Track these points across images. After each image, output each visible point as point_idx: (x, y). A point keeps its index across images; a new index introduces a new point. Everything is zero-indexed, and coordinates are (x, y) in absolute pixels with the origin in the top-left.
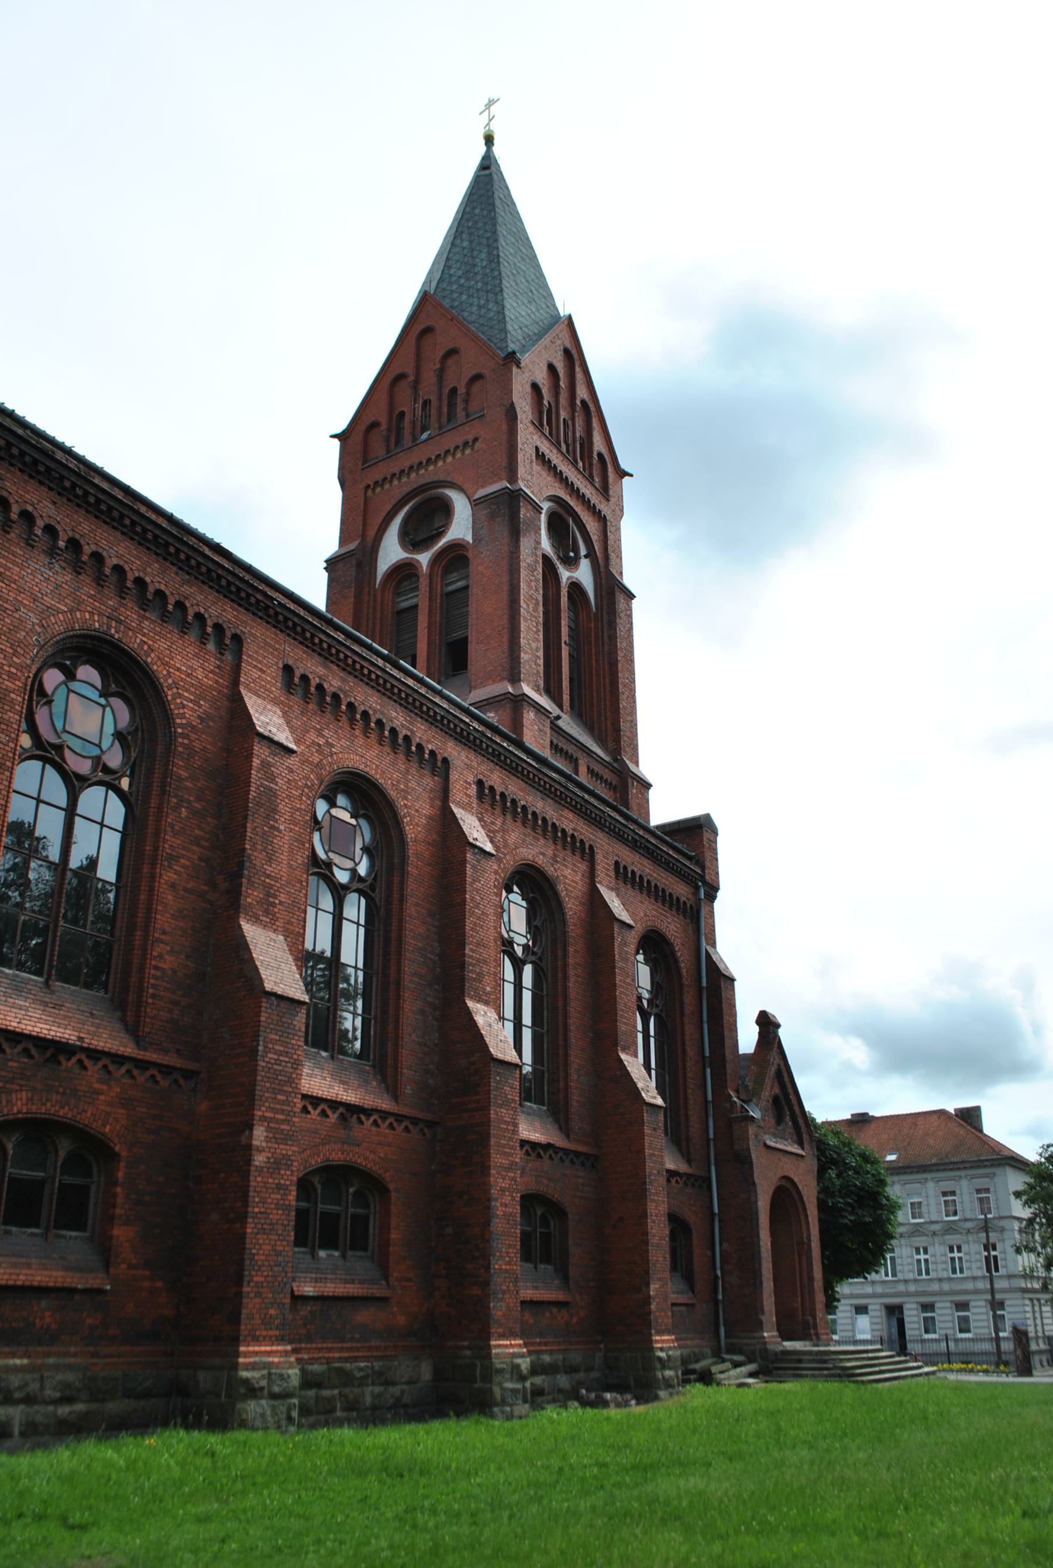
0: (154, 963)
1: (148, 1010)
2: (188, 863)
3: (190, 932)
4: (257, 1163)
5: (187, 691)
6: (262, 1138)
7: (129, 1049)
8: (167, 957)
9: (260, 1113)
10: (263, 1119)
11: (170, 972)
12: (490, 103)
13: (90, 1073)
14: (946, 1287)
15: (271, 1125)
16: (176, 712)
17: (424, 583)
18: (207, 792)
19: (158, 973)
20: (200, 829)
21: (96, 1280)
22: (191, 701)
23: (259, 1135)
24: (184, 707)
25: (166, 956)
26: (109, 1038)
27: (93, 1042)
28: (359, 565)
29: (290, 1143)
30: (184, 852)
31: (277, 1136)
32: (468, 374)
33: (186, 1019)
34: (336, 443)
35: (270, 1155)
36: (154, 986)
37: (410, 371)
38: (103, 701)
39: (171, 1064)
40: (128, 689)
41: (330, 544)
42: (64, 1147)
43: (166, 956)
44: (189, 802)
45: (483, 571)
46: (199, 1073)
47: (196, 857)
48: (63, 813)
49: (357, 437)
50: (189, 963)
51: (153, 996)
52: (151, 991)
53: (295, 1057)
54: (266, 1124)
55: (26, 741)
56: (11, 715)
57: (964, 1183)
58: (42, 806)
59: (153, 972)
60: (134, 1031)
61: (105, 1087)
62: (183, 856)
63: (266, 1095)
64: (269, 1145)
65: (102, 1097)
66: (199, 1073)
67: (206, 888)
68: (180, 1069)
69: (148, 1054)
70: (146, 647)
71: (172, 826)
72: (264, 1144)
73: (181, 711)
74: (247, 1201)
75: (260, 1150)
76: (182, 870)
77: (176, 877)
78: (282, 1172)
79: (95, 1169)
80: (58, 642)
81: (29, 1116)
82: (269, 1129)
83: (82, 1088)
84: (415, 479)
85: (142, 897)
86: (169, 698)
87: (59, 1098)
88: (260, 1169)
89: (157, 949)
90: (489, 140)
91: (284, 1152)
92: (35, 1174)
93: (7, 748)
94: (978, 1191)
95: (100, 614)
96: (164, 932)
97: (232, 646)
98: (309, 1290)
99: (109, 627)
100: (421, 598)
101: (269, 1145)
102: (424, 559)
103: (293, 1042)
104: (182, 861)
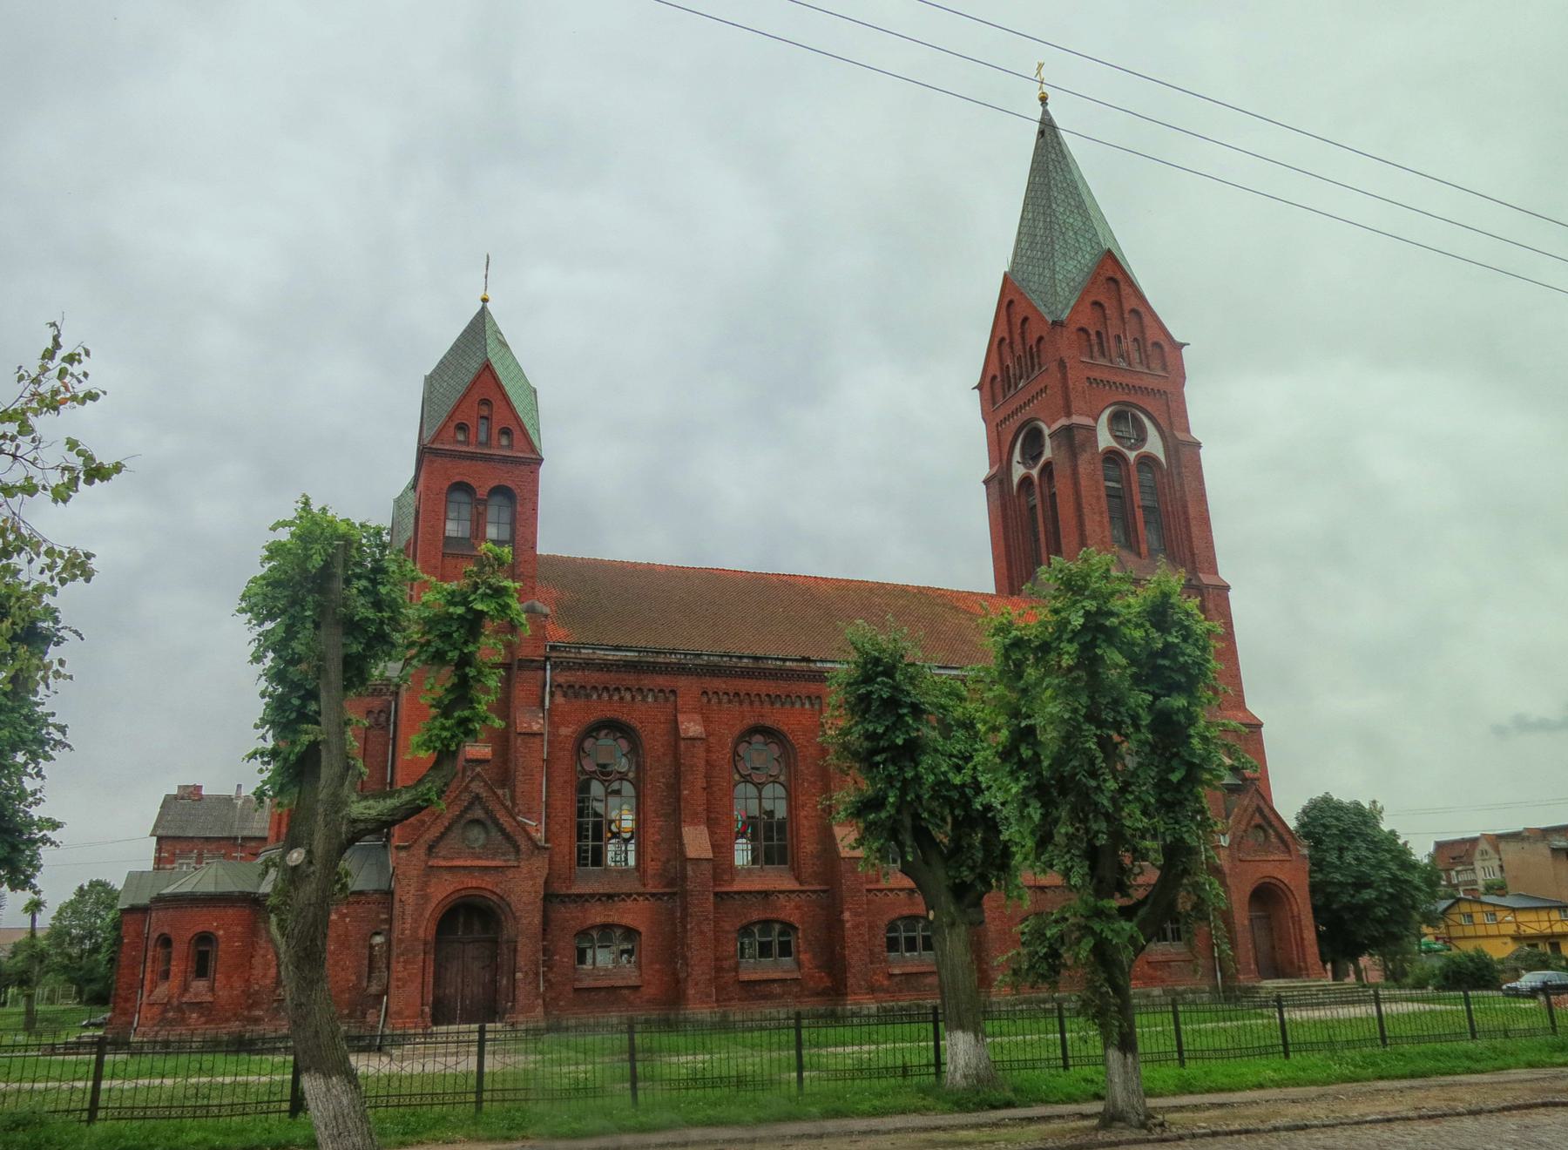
7: (797, 887)
12: (1041, 66)
17: (1037, 490)
21: (796, 975)
23: (847, 915)
26: (789, 884)
28: (1001, 482)
32: (1036, 336)
34: (977, 392)
37: (1006, 335)
41: (984, 470)
42: (777, 927)
45: (1062, 485)
49: (987, 387)
55: (737, 777)
74: (237, 1052)
98: (897, 971)
100: (1037, 500)
102: (1035, 472)
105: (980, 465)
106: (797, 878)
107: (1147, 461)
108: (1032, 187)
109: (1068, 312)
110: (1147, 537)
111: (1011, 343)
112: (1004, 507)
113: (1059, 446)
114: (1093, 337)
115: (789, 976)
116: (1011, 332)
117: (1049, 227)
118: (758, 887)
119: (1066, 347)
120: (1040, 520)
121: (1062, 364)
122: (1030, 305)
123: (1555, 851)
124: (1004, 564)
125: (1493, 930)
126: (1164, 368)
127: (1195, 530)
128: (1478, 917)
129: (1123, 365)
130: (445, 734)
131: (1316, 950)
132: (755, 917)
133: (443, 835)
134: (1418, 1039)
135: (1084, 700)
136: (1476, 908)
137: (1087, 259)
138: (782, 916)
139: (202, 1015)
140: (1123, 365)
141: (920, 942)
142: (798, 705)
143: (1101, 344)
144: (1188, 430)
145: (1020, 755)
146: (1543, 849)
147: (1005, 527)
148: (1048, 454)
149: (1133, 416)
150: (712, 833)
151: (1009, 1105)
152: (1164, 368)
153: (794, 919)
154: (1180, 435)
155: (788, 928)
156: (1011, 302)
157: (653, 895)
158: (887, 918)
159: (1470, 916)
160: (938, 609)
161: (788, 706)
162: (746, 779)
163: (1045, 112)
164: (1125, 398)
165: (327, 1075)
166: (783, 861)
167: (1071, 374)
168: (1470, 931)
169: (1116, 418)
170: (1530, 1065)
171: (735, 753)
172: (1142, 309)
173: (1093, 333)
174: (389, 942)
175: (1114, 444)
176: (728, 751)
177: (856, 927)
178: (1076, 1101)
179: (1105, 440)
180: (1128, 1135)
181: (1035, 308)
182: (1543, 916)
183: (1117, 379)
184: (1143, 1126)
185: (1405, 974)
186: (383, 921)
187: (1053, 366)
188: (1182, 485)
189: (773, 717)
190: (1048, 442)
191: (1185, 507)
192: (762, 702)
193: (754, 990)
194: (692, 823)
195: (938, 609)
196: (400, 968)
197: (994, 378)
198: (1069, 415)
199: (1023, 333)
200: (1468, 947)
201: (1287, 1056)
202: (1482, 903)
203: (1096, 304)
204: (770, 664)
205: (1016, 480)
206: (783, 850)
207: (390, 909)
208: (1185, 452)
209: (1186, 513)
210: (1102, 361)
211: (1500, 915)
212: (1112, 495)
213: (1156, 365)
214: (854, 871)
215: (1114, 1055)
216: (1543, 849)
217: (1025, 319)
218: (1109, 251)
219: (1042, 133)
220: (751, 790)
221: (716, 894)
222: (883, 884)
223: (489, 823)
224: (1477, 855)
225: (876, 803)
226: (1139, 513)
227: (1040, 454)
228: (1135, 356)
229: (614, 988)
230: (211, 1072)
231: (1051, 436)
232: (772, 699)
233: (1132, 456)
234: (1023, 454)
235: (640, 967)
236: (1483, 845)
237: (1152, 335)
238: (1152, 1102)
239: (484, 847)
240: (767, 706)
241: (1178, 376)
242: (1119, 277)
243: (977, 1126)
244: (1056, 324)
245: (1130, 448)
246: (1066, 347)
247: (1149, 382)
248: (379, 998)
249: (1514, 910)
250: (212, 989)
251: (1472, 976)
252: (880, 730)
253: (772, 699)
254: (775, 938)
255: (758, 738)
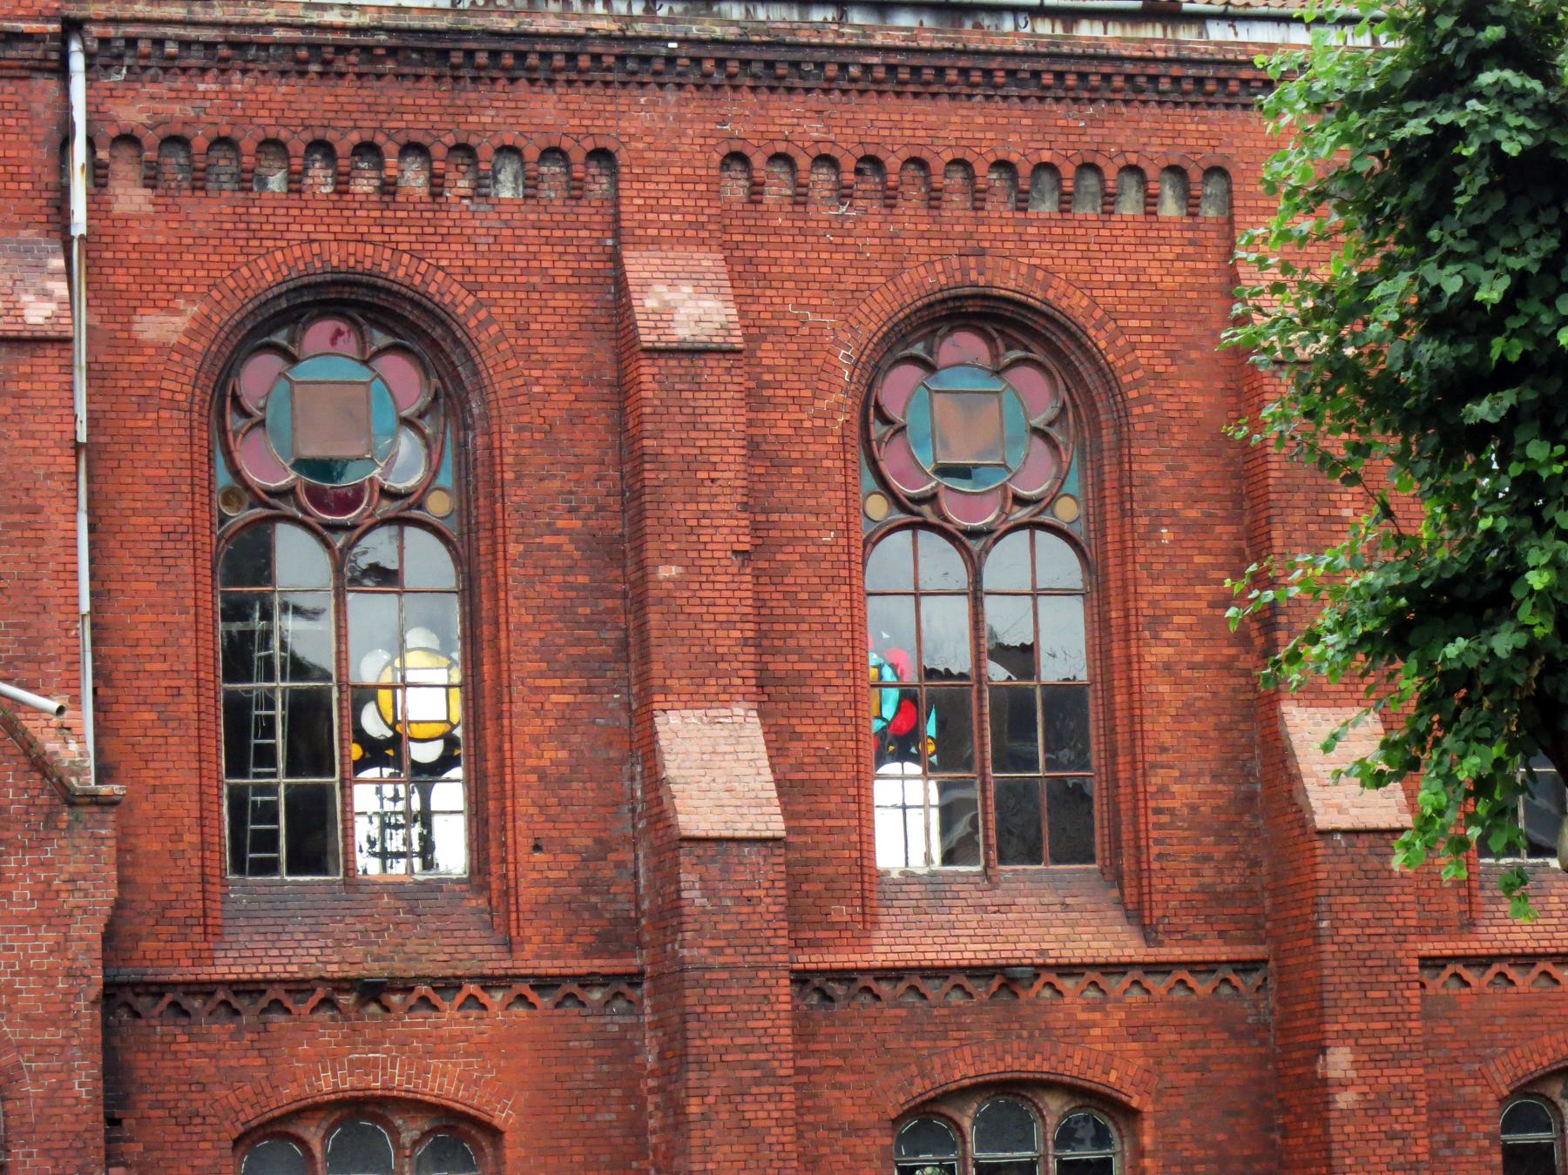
0: (1152, 804)
1: (1155, 881)
2: (1188, 620)
3: (1212, 734)
4: (1342, 1105)
5: (1133, 316)
6: (1346, 1065)
7: (1131, 948)
8: (1175, 788)
9: (1336, 1027)
10: (1344, 1036)
11: (1186, 811)
13: (1068, 1000)
15: (1363, 1041)
16: (1120, 364)
18: (1206, 483)
19: (1165, 819)
20: (1203, 551)
22: (1146, 331)
23: (1339, 1061)
24: (1133, 347)
25: (1180, 782)
26: (1112, 940)
27: (1064, 953)
29: (1405, 1063)
30: (1179, 604)
31: (1373, 1056)
33: (1228, 880)
35: (1366, 1089)
36: (1158, 842)
38: (996, 385)
39: (1209, 958)
40: (1033, 346)
43: (1180, 782)
44: (1174, 513)
46: (1266, 962)
47: (1204, 604)
48: (964, 599)
50: (1220, 787)
51: (1160, 856)
52: (1155, 850)
53: (1398, 922)
54: (1352, 1042)
55: (878, 507)
56: (832, 494)
58: (924, 600)
59: (1152, 818)
60: (1138, 916)
61: (1097, 1016)
62: (1178, 612)
63: (1346, 995)
64: (1363, 1073)
65: (1096, 1032)
66: (1266, 962)
67: (1233, 651)
68: (1228, 962)
69: (1162, 950)
70: (1040, 275)
71: (1148, 566)
72: (1352, 1074)
73: (1129, 358)
75: (1344, 1085)
76: (1181, 635)
77: (1170, 650)
78: (1395, 1112)
79: (1114, 1134)
80: (886, 334)
81: (980, 1079)
82: (1357, 1047)
83: (1059, 1025)
85: (1118, 699)
86: (1102, 344)
87: (1023, 1045)
88: (1348, 1114)
89: (1153, 780)
91: (1396, 1080)
92: (1017, 1154)
93: (835, 549)
95: (943, 257)
96: (1164, 750)
99: (965, 271)
101: (1363, 1073)
103: (1392, 899)
104: (1177, 619)
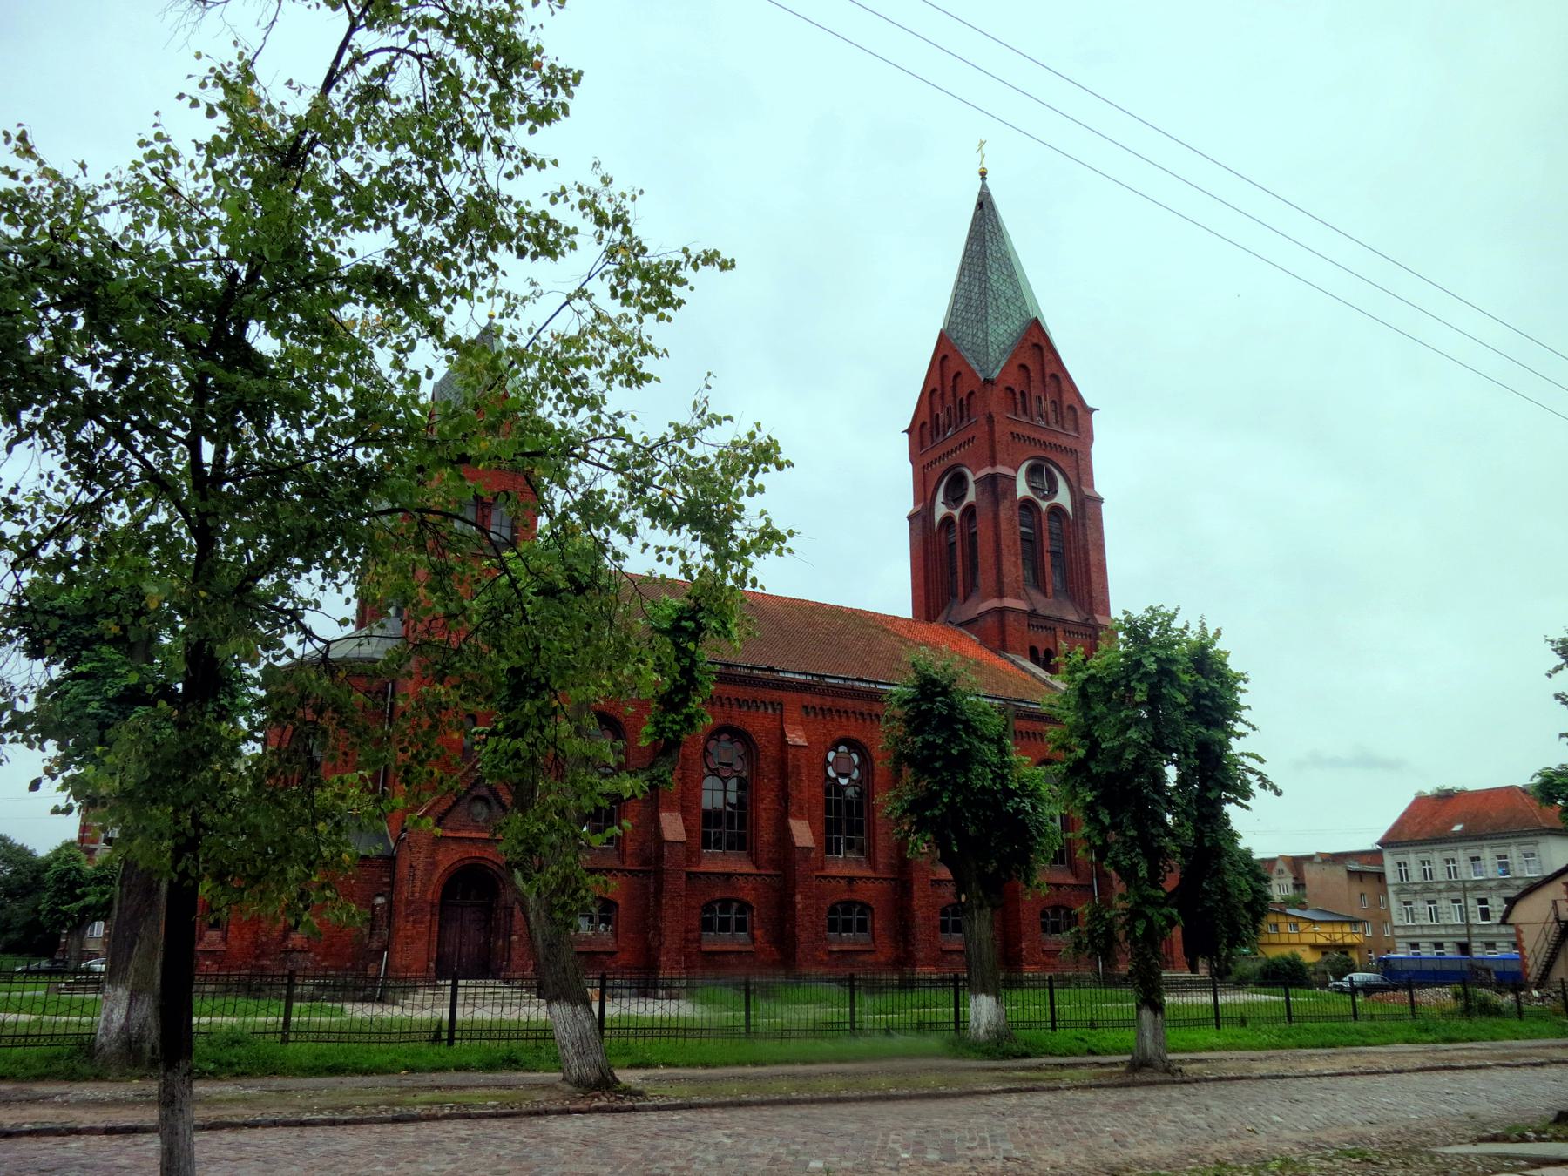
7: (753, 870)
12: (982, 143)
14: (1426, 932)
23: (798, 898)
26: (748, 868)
28: (924, 519)
31: (806, 897)
41: (908, 505)
42: (735, 905)
43: (766, 835)
45: (982, 527)
57: (1436, 854)
84: (947, 462)
90: (983, 174)
94: (1499, 857)
97: (778, 705)
100: (956, 536)
102: (957, 513)
105: (906, 503)
106: (755, 863)
107: (1057, 511)
108: (968, 253)
109: (998, 372)
110: (1053, 579)
111: (943, 394)
112: (925, 541)
113: (983, 492)
114: (1018, 396)
115: (743, 949)
116: (942, 385)
117: (984, 292)
118: (721, 870)
119: (995, 402)
120: (959, 559)
121: (990, 419)
122: (964, 362)
123: (1350, 873)
124: (922, 593)
125: (1295, 939)
126: (1077, 429)
127: (1094, 577)
128: (1282, 927)
129: (1042, 423)
130: (677, 727)
131: (1181, 946)
132: (718, 895)
133: (451, 809)
134: (1317, 1019)
135: (1150, 729)
136: (1282, 919)
137: (1016, 325)
138: (740, 895)
139: (215, 962)
140: (1042, 423)
141: (855, 924)
142: (762, 709)
143: (1024, 404)
144: (1092, 486)
145: (1089, 770)
146: (1340, 872)
147: (926, 559)
148: (971, 496)
149: (1050, 473)
150: (684, 819)
151: (1026, 1055)
152: (1077, 429)
153: (750, 897)
154: (1086, 491)
155: (745, 907)
156: (945, 357)
157: (630, 872)
158: (829, 902)
159: (1276, 926)
160: (872, 631)
161: (753, 710)
162: (714, 773)
163: (984, 186)
164: (1042, 454)
165: (574, 1004)
166: (742, 848)
167: (997, 428)
168: (1274, 939)
169: (1032, 471)
170: (1407, 1042)
171: (706, 749)
172: (1060, 375)
173: (1017, 391)
174: (390, 903)
175: (1030, 494)
176: (700, 746)
177: (806, 908)
178: (1075, 1055)
179: (1022, 489)
180: (1158, 1077)
181: (968, 366)
182: (1337, 929)
183: (1036, 436)
184: (1167, 1071)
185: (1229, 972)
186: (386, 884)
187: (983, 419)
188: (1085, 535)
189: (740, 719)
190: (972, 488)
191: (1086, 553)
192: (731, 705)
193: (713, 960)
194: (669, 810)
195: (872, 631)
196: (409, 926)
197: (924, 424)
198: (993, 464)
199: (954, 387)
200: (1286, 952)
201: (1218, 1027)
202: (1287, 915)
203: (1023, 366)
204: (740, 671)
205: (938, 518)
206: (742, 838)
207: (392, 874)
208: (1088, 505)
209: (1087, 559)
210: (1024, 419)
211: (1302, 926)
212: (1025, 539)
213: (1069, 425)
214: (807, 859)
215: (1147, 1014)
216: (1340, 872)
217: (958, 374)
218: (1036, 319)
219: (980, 205)
220: (718, 783)
221: (688, 874)
222: (827, 872)
223: (492, 799)
224: (1274, 874)
225: (931, 799)
226: (1047, 557)
227: (963, 496)
228: (1052, 417)
229: (595, 953)
230: (246, 1013)
231: (976, 482)
232: (740, 703)
233: (1044, 505)
234: (946, 495)
235: (616, 936)
236: (1280, 865)
237: (1068, 399)
238: (1170, 1056)
239: (486, 821)
240: (735, 708)
241: (1087, 437)
242: (1043, 343)
243: (1023, 1069)
244: (988, 382)
245: (1044, 498)
246: (995, 402)
247: (1064, 441)
248: (379, 954)
249: (1314, 922)
250: (225, 939)
251: (1285, 975)
252: (939, 741)
253: (740, 703)
254: (733, 915)
255: (725, 737)
